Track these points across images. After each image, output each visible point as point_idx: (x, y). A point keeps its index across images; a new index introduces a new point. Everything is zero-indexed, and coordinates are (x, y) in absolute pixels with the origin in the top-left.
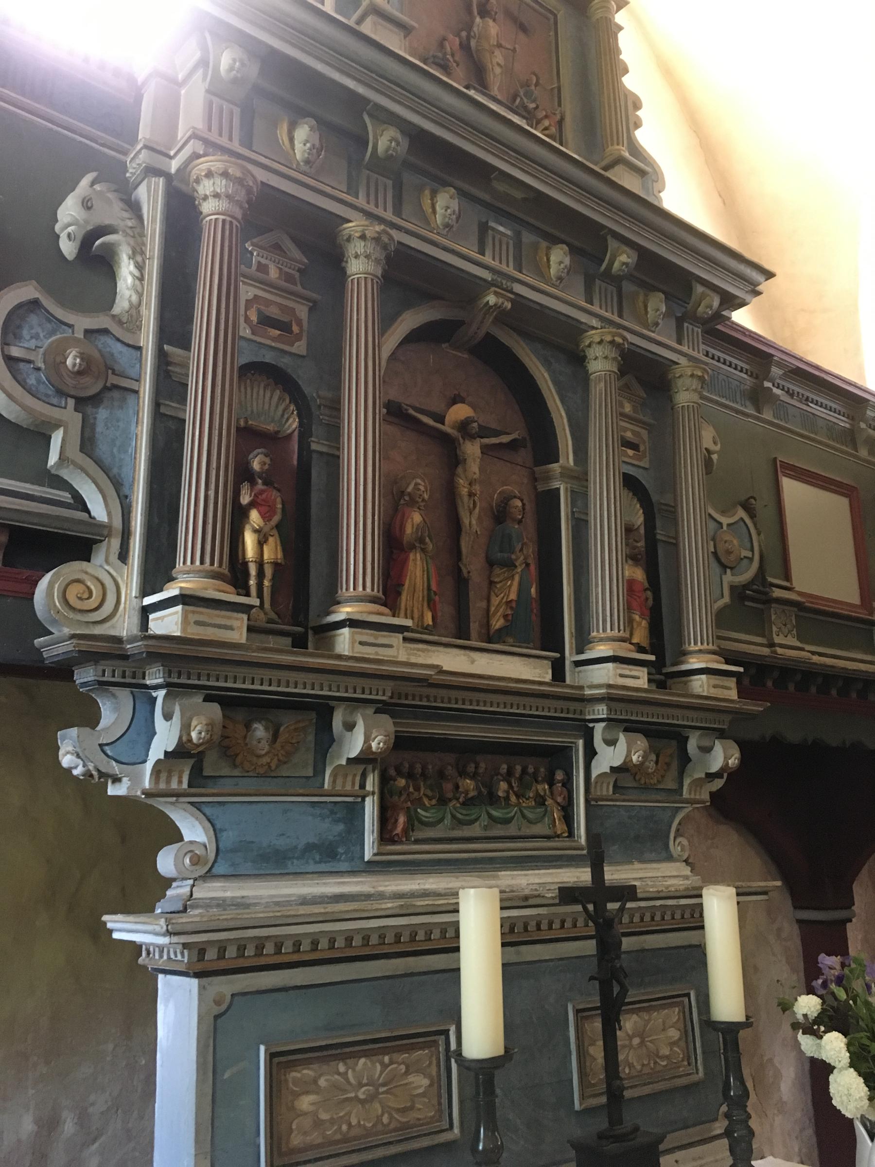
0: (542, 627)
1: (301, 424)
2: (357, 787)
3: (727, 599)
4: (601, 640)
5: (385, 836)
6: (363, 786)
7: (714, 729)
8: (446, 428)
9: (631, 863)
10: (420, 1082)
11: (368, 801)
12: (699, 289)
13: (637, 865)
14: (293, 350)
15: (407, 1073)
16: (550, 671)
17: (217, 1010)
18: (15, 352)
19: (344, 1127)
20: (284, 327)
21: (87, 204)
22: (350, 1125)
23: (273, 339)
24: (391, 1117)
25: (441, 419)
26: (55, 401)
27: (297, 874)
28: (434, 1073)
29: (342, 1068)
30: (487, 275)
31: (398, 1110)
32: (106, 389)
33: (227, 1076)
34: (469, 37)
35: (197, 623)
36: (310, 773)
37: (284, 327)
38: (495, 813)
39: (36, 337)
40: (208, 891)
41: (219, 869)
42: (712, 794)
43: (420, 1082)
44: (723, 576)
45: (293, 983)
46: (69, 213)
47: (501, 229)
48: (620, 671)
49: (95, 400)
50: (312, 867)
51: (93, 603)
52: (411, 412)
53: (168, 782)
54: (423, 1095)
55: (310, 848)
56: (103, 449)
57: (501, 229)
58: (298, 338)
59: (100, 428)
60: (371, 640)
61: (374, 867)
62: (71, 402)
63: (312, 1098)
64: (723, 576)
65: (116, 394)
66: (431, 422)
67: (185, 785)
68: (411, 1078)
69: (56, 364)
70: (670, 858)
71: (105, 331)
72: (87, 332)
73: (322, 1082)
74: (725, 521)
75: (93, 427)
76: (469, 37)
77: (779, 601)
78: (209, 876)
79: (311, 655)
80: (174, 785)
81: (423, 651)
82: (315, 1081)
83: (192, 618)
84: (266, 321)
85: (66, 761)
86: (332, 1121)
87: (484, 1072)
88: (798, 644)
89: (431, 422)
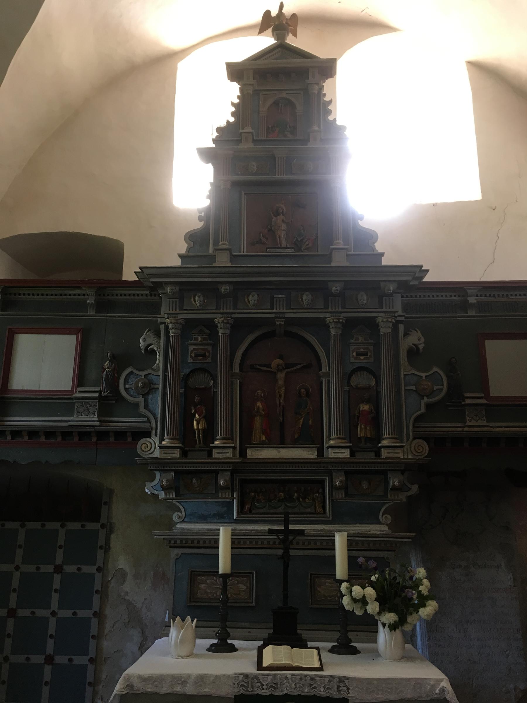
0: (313, 437)
1: (214, 383)
2: (230, 496)
3: (423, 410)
4: (333, 439)
5: (241, 510)
6: (233, 496)
7: (398, 470)
8: (273, 370)
9: (356, 524)
10: (243, 587)
11: (235, 500)
12: (382, 284)
13: (358, 525)
14: (207, 361)
15: (238, 584)
16: (316, 452)
17: (176, 557)
18: (127, 386)
19: (215, 595)
20: (204, 355)
21: (144, 340)
22: (217, 595)
23: (200, 360)
24: (231, 595)
25: (269, 366)
26: (137, 396)
27: (210, 522)
28: (248, 585)
29: (215, 578)
30: (273, 316)
31: (234, 594)
32: (150, 389)
33: (179, 574)
34: (271, 227)
35: (164, 453)
36: (214, 492)
37: (204, 355)
38: (288, 505)
39: (133, 381)
40: (184, 526)
41: (186, 520)
42: (408, 497)
43: (243, 587)
44: (422, 401)
45: (199, 553)
46: (142, 344)
47: (280, 296)
48: (333, 451)
49: (148, 393)
50: (216, 520)
51: (148, 449)
52: (258, 367)
53: (169, 496)
54: (244, 591)
55: (214, 515)
56: (151, 406)
57: (280, 296)
58: (209, 357)
59: (149, 401)
60: (221, 452)
61: (237, 522)
62: (141, 396)
63: (204, 585)
64: (422, 401)
65: (154, 390)
66: (265, 369)
67: (344, 496)
68: (239, 585)
69: (136, 386)
70: (380, 523)
71: (150, 374)
72: (145, 375)
73: (208, 581)
74: (424, 375)
75: (148, 401)
76: (271, 227)
77: (470, 405)
78: (183, 522)
79: (189, 459)
80: (171, 497)
81: (258, 450)
82: (206, 581)
83: (163, 452)
84: (197, 355)
85: (147, 490)
86: (211, 592)
87: (225, 576)
88: (487, 424)
89: (265, 369)
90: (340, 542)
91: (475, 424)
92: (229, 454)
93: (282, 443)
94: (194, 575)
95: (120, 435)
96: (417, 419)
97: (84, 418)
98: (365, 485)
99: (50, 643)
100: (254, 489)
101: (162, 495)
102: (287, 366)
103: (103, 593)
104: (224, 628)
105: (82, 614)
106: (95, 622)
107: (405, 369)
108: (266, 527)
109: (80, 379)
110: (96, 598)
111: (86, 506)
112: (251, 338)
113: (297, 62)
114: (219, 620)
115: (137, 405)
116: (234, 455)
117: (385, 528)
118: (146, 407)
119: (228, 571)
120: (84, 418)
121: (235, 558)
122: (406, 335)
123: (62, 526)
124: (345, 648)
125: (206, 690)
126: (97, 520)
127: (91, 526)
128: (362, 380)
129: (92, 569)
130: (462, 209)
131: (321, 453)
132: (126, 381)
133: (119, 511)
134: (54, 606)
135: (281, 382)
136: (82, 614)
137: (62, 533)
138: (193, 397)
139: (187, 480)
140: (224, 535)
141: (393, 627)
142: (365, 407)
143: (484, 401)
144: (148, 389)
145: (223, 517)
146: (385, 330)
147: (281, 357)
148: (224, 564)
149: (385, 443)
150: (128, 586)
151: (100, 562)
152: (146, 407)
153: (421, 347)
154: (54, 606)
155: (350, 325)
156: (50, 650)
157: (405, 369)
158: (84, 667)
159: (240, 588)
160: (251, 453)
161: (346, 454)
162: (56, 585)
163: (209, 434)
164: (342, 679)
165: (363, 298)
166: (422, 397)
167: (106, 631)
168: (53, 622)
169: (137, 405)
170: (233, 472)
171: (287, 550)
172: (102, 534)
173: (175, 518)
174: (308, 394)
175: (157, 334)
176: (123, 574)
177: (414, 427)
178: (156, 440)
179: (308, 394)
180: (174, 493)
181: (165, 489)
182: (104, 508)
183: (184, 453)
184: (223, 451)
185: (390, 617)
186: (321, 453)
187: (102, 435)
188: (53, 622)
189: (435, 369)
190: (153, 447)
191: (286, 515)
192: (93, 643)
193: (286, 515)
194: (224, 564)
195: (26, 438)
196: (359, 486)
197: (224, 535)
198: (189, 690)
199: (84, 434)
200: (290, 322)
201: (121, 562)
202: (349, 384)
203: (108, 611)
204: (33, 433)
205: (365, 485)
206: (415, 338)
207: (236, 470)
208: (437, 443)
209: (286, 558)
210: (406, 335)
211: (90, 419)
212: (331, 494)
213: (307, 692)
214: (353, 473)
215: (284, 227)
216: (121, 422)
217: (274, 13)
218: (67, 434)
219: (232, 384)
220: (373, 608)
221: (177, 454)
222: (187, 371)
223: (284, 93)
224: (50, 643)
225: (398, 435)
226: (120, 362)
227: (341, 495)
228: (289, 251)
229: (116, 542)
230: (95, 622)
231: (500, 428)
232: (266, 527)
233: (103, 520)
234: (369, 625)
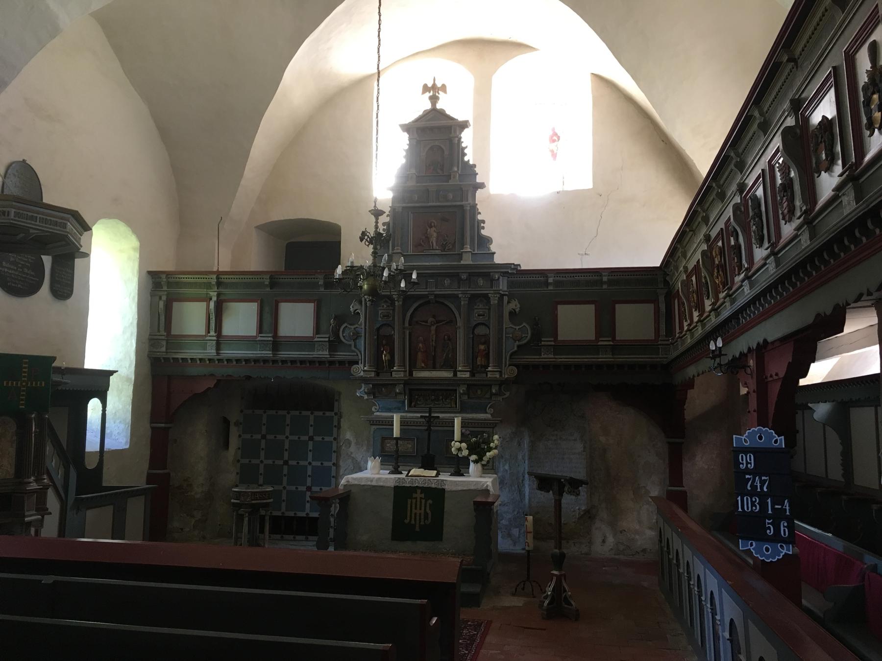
0: (450, 364)
3: (516, 349)
5: (410, 405)
20: (388, 316)
25: (426, 322)
37: (388, 316)
40: (378, 414)
46: (352, 309)
87: (397, 439)
90: (457, 422)
91: (547, 357)
92: (402, 375)
93: (434, 368)
94: (384, 439)
95: (341, 363)
96: (511, 355)
97: (320, 353)
98: (479, 392)
99: (309, 480)
100: (417, 394)
101: (366, 397)
102: (438, 322)
103: (338, 452)
104: (397, 463)
105: (326, 464)
106: (334, 468)
107: (507, 323)
108: (419, 415)
109: (318, 330)
110: (334, 455)
111: (324, 402)
112: (415, 305)
113: (443, 122)
114: (394, 459)
115: (350, 345)
116: (405, 376)
117: (489, 416)
118: (355, 346)
119: (399, 436)
120: (320, 353)
121: (402, 431)
122: (509, 302)
123: (312, 413)
124: (458, 473)
125: (381, 484)
126: (333, 411)
127: (328, 414)
128: (480, 331)
129: (331, 439)
130: (577, 195)
131: (455, 375)
132: (343, 332)
133: (345, 406)
134: (310, 459)
135: (433, 332)
136: (326, 464)
137: (312, 418)
138: (381, 341)
139: (379, 389)
140: (396, 418)
141: (476, 462)
142: (482, 347)
143: (553, 343)
144: (356, 336)
145: (398, 410)
146: (494, 301)
147: (434, 317)
148: (396, 433)
149: (490, 369)
150: (353, 448)
151: (335, 435)
152: (355, 346)
153: (517, 310)
154: (310, 459)
155: (473, 298)
156: (309, 484)
157: (507, 323)
158: (330, 468)
159: (407, 447)
160: (418, 374)
161: (467, 375)
162: (310, 447)
163: (391, 363)
164: (443, 481)
165: (481, 282)
166: (515, 341)
167: (341, 473)
168: (309, 468)
169: (350, 345)
170: (405, 384)
171: (429, 426)
172: (336, 418)
173: (373, 409)
174: (449, 339)
175: (360, 303)
176: (349, 443)
177: (510, 358)
178: (362, 366)
179: (449, 339)
180: (92, 443)
181: (368, 394)
182: (336, 404)
183: (378, 374)
184: (398, 373)
185: (473, 457)
186: (455, 375)
187: (331, 363)
188: (309, 468)
189: (524, 324)
190: (361, 370)
191: (430, 408)
192: (333, 480)
193: (430, 408)
194: (396, 433)
195: (289, 364)
196: (476, 393)
197: (396, 418)
198: (374, 483)
199: (321, 363)
200: (436, 296)
201: (349, 435)
202: (473, 333)
203: (341, 463)
204: (293, 362)
205: (479, 392)
206: (515, 305)
207: (406, 383)
208: (523, 368)
209: (429, 430)
210: (509, 302)
211: (324, 354)
212: (460, 397)
213: (426, 485)
214: (471, 386)
215: (435, 235)
216: (341, 355)
217: (430, 85)
218: (312, 362)
219: (404, 333)
220: (465, 453)
221: (373, 374)
222: (378, 326)
223: (437, 140)
224: (309, 480)
225: (499, 364)
226: (340, 319)
227: (466, 397)
228: (438, 252)
229: (344, 424)
230: (334, 468)
231: (563, 359)
232: (419, 415)
233: (336, 410)
234: (465, 462)
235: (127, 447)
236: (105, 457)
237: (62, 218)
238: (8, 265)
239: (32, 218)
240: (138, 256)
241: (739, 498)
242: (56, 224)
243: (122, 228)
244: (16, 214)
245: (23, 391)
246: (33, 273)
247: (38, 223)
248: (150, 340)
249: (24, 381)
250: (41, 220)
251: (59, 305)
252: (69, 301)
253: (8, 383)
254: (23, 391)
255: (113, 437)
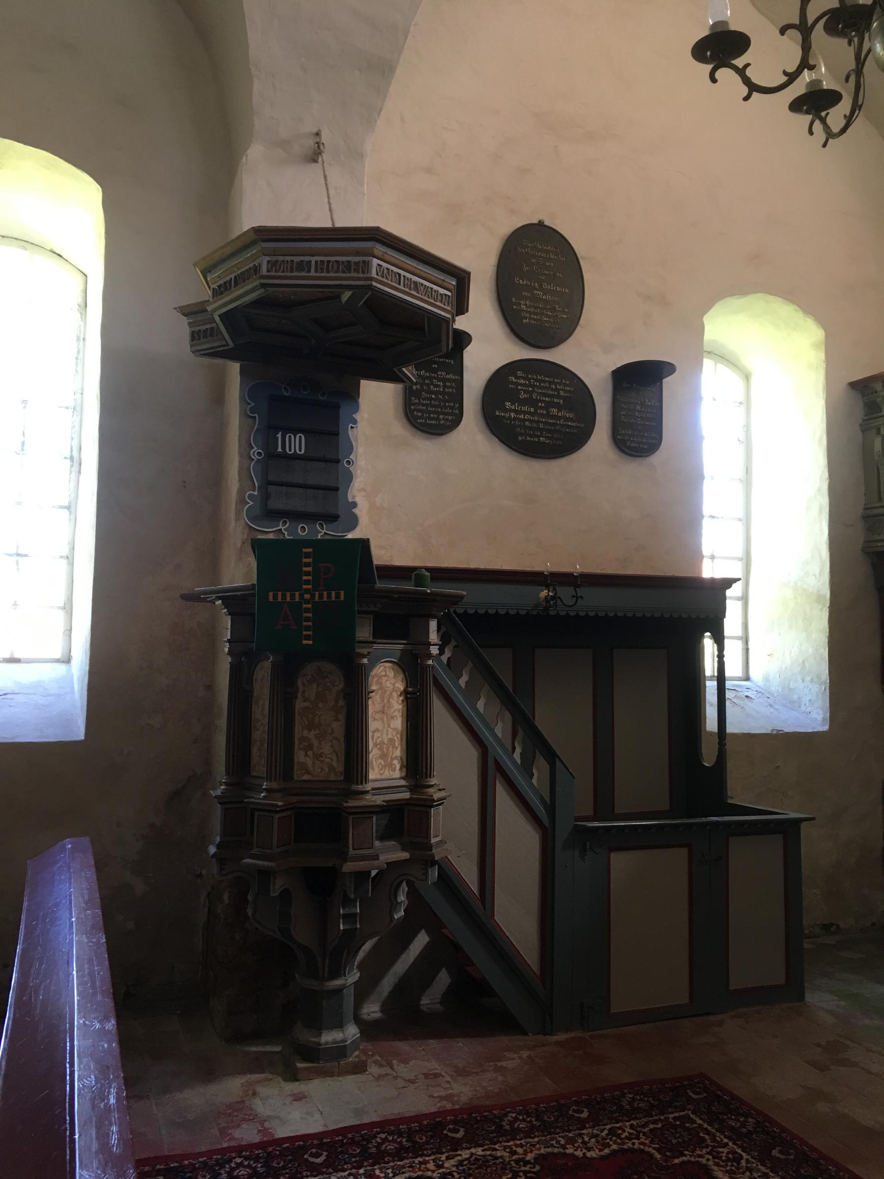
235: (826, 728)
236: (729, 747)
237: (358, 253)
238: (516, 407)
239: (301, 266)
240: (822, 356)
241: (279, 435)
242: (348, 266)
243: (786, 310)
244: (272, 265)
245: (307, 610)
246: (571, 415)
247: (313, 273)
248: (865, 518)
249: (307, 591)
250: (320, 266)
251: (633, 468)
252: (656, 458)
253: (275, 597)
254: (307, 610)
255: (803, 708)
